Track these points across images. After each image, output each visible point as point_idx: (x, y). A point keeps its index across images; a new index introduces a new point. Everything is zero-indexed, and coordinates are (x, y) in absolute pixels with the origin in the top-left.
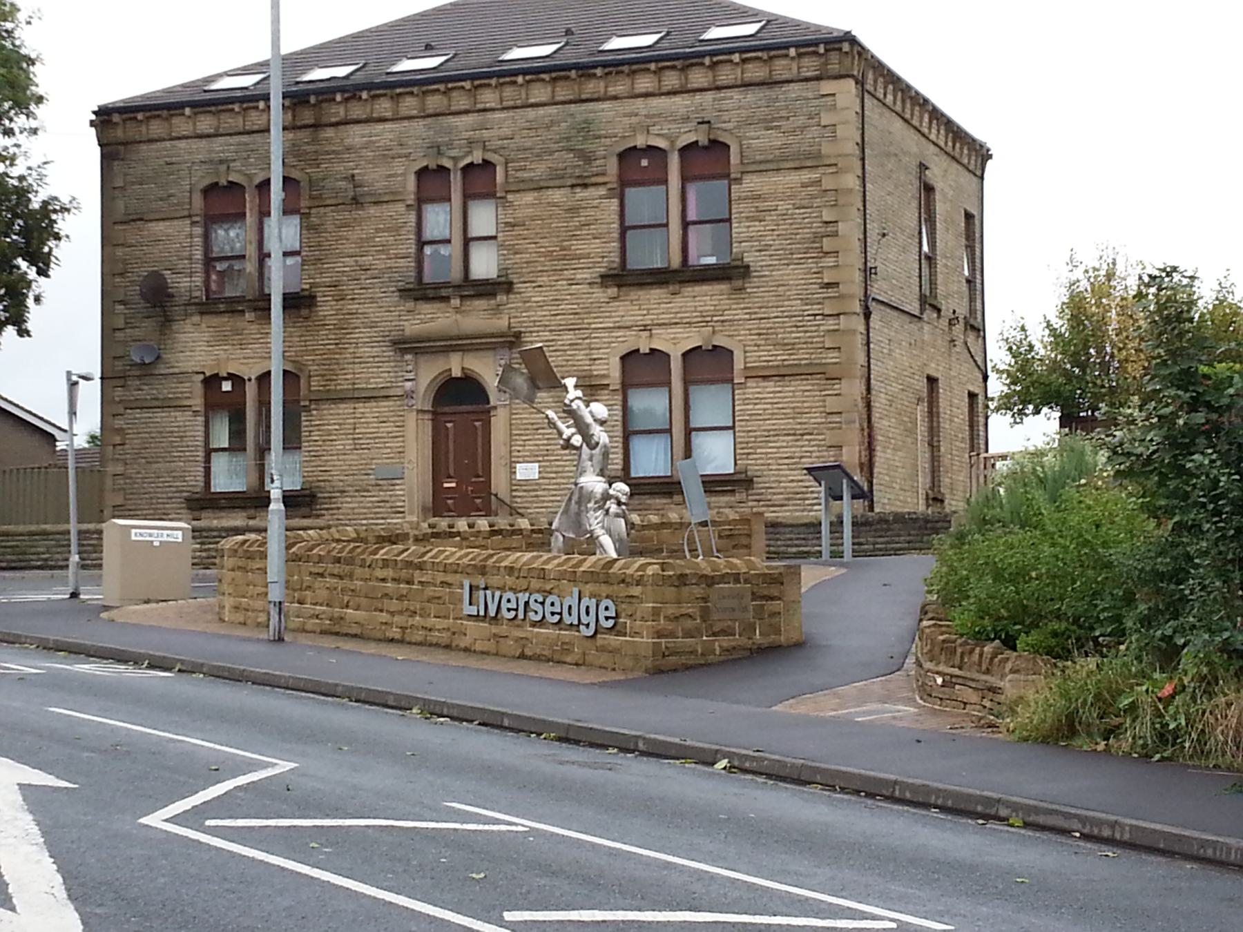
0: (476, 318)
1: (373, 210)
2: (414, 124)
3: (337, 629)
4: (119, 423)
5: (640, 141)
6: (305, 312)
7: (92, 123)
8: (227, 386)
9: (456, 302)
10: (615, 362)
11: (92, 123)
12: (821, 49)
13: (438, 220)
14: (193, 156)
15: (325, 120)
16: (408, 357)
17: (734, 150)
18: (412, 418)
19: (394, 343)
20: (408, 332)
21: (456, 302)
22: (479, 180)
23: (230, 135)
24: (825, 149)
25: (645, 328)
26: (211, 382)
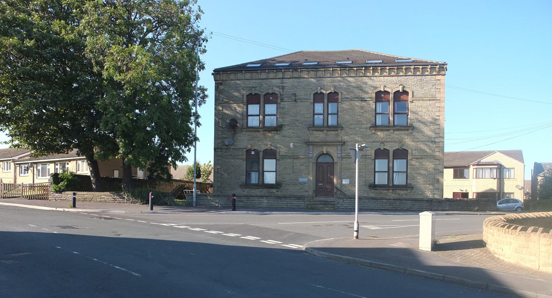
0: (331, 136)
1: (300, 103)
2: (394, 77)
3: (9, 194)
4: (219, 162)
5: (271, 92)
6: (279, 132)
7: (213, 74)
8: (253, 153)
9: (325, 132)
10: (373, 152)
11: (213, 74)
12: (364, 68)
13: (319, 108)
14: (242, 85)
15: (285, 77)
16: (311, 147)
17: (340, 94)
18: (311, 164)
19: (306, 143)
20: (311, 140)
21: (325, 132)
22: (271, 98)
23: (256, 79)
24: (438, 95)
25: (382, 143)
26: (248, 151)
